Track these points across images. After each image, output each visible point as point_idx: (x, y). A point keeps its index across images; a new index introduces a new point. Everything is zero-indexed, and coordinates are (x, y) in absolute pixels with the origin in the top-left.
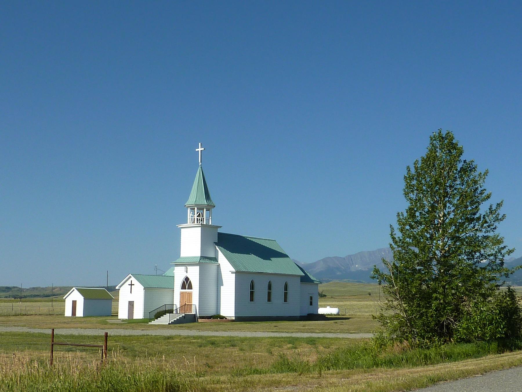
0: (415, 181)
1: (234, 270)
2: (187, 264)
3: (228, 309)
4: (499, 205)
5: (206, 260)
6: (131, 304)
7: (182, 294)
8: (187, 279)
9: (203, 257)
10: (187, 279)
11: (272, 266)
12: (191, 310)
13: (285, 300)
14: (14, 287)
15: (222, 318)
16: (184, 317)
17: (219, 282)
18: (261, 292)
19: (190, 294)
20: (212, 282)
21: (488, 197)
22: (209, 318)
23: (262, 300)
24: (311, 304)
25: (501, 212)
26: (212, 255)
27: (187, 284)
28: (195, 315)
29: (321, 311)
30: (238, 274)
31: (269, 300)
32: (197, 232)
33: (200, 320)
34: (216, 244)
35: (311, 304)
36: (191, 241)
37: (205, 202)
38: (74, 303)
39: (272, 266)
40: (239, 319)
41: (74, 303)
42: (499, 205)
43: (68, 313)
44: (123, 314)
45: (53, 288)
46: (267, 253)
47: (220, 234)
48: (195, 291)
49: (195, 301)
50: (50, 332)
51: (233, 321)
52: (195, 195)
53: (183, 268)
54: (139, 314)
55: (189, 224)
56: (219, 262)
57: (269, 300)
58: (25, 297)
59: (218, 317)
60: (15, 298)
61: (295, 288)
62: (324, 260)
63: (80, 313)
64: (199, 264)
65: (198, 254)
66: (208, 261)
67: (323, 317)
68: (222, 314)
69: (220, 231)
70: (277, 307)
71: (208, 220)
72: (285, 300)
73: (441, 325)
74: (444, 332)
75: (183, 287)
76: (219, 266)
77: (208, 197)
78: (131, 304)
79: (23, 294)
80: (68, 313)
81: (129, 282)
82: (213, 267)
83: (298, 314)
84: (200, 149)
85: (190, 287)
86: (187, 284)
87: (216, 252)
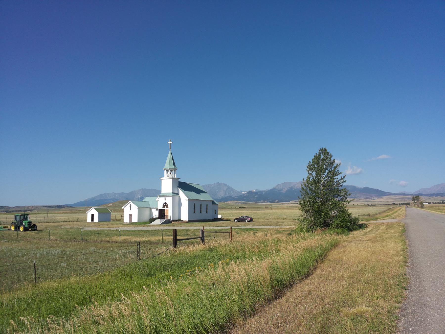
0: (311, 168)
1: (188, 199)
2: (165, 196)
3: (185, 216)
4: (344, 177)
5: (175, 194)
6: (131, 215)
8: (165, 203)
9: (173, 193)
10: (165, 203)
11: (201, 197)
12: (168, 218)
14: (6, 206)
15: (182, 221)
16: (166, 221)
17: (180, 204)
20: (178, 205)
21: (341, 173)
22: (176, 221)
23: (203, 212)
25: (345, 179)
26: (176, 192)
29: (219, 217)
30: (190, 201)
32: (171, 181)
33: (173, 222)
36: (167, 185)
37: (174, 167)
38: (93, 215)
39: (201, 197)
40: (190, 221)
41: (93, 215)
42: (344, 177)
44: (126, 220)
45: (29, 207)
46: (199, 192)
47: (179, 182)
50: (230, 228)
51: (187, 222)
52: (168, 164)
53: (164, 198)
54: (135, 220)
55: (165, 177)
58: (13, 211)
59: (179, 220)
60: (7, 212)
63: (96, 219)
64: (172, 196)
65: (171, 192)
66: (175, 195)
67: (220, 220)
68: (182, 219)
69: (179, 180)
70: (204, 216)
71: (174, 176)
73: (325, 222)
74: (326, 225)
76: (179, 197)
77: (174, 165)
78: (131, 215)
79: (10, 210)
80: (89, 220)
81: (129, 205)
82: (177, 197)
83: (211, 218)
84: (170, 142)
85: (167, 207)
87: (178, 190)
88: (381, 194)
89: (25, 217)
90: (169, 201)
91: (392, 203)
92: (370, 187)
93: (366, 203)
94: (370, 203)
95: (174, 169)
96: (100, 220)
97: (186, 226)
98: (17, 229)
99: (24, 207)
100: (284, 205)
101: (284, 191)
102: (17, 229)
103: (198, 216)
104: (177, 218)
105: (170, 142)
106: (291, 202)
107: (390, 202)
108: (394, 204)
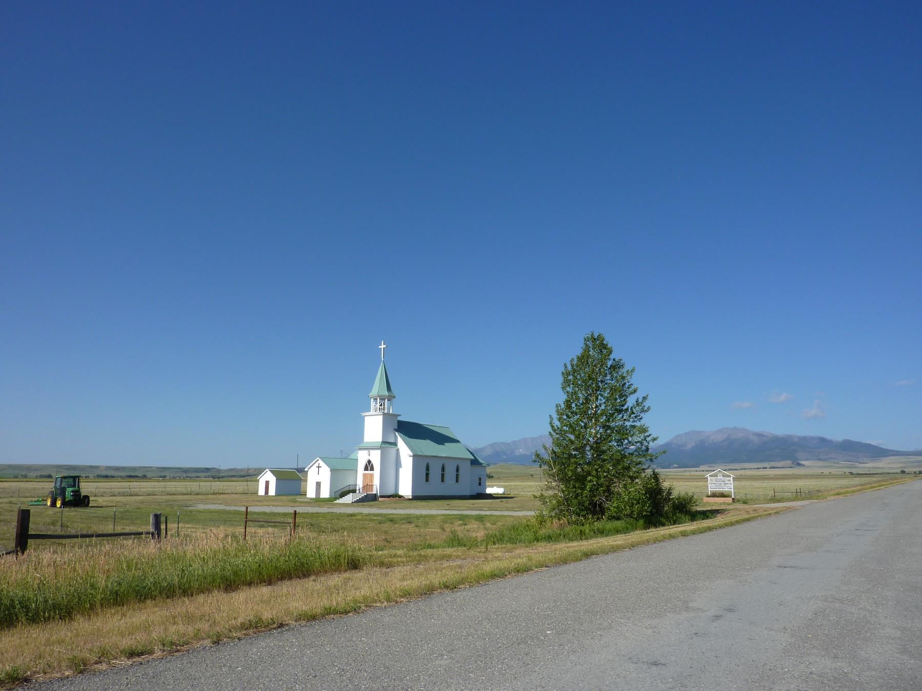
0: (571, 377)
3: (406, 489)
4: (644, 398)
5: (387, 445)
6: (318, 485)
7: (364, 475)
8: (369, 462)
9: (384, 442)
10: (369, 462)
13: (457, 481)
15: (400, 497)
16: (366, 496)
17: (398, 464)
18: (435, 474)
19: (372, 476)
20: (391, 465)
21: (635, 391)
22: (389, 497)
24: (480, 484)
25: (646, 404)
26: (393, 441)
27: (369, 466)
28: (376, 495)
29: (489, 491)
30: (416, 457)
31: (443, 481)
34: (396, 430)
35: (480, 484)
36: (373, 427)
37: (387, 393)
38: (267, 483)
40: (416, 498)
41: (267, 483)
42: (644, 398)
43: (261, 492)
44: (311, 493)
45: (249, 470)
46: (440, 439)
48: (377, 473)
49: (376, 482)
50: (244, 509)
52: (378, 387)
53: (366, 452)
54: (325, 493)
56: (399, 446)
57: (443, 481)
59: (397, 496)
61: (466, 469)
62: (492, 445)
63: (272, 492)
64: (380, 448)
65: (380, 440)
67: (490, 497)
68: (401, 493)
69: (399, 418)
70: (450, 487)
71: (389, 409)
72: (457, 481)
75: (366, 469)
76: (398, 450)
77: (389, 388)
78: (318, 485)
79: (221, 474)
80: (261, 492)
81: (317, 465)
82: (392, 451)
83: (467, 493)
84: (383, 346)
85: (372, 469)
86: (369, 466)
87: (396, 437)
88: (878, 452)
89: (75, 480)
90: (376, 457)
91: (899, 471)
92: (855, 438)
93: (847, 470)
94: (854, 471)
95: (390, 395)
96: (278, 493)
97: (407, 508)
98: (54, 504)
99: (241, 470)
100: (687, 474)
101: (689, 447)
102: (54, 504)
103: (436, 487)
104: (391, 491)
105: (383, 346)
106: (702, 468)
107: (898, 468)
108: (903, 472)
